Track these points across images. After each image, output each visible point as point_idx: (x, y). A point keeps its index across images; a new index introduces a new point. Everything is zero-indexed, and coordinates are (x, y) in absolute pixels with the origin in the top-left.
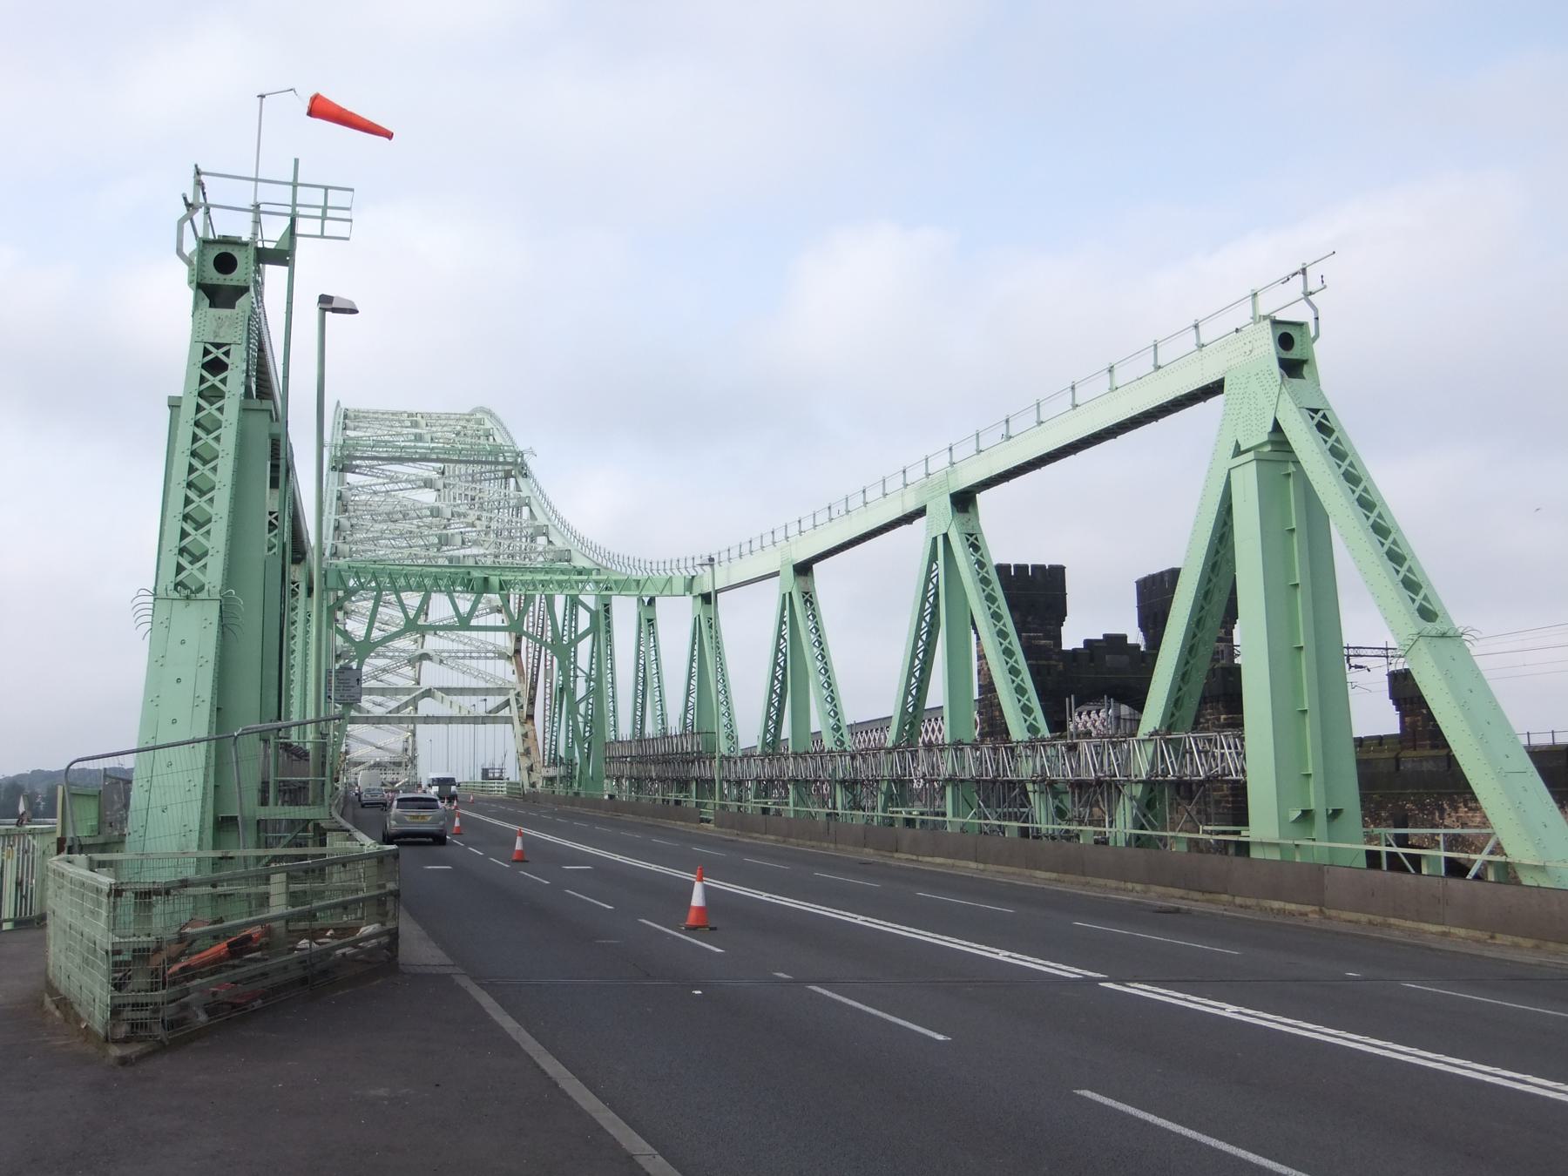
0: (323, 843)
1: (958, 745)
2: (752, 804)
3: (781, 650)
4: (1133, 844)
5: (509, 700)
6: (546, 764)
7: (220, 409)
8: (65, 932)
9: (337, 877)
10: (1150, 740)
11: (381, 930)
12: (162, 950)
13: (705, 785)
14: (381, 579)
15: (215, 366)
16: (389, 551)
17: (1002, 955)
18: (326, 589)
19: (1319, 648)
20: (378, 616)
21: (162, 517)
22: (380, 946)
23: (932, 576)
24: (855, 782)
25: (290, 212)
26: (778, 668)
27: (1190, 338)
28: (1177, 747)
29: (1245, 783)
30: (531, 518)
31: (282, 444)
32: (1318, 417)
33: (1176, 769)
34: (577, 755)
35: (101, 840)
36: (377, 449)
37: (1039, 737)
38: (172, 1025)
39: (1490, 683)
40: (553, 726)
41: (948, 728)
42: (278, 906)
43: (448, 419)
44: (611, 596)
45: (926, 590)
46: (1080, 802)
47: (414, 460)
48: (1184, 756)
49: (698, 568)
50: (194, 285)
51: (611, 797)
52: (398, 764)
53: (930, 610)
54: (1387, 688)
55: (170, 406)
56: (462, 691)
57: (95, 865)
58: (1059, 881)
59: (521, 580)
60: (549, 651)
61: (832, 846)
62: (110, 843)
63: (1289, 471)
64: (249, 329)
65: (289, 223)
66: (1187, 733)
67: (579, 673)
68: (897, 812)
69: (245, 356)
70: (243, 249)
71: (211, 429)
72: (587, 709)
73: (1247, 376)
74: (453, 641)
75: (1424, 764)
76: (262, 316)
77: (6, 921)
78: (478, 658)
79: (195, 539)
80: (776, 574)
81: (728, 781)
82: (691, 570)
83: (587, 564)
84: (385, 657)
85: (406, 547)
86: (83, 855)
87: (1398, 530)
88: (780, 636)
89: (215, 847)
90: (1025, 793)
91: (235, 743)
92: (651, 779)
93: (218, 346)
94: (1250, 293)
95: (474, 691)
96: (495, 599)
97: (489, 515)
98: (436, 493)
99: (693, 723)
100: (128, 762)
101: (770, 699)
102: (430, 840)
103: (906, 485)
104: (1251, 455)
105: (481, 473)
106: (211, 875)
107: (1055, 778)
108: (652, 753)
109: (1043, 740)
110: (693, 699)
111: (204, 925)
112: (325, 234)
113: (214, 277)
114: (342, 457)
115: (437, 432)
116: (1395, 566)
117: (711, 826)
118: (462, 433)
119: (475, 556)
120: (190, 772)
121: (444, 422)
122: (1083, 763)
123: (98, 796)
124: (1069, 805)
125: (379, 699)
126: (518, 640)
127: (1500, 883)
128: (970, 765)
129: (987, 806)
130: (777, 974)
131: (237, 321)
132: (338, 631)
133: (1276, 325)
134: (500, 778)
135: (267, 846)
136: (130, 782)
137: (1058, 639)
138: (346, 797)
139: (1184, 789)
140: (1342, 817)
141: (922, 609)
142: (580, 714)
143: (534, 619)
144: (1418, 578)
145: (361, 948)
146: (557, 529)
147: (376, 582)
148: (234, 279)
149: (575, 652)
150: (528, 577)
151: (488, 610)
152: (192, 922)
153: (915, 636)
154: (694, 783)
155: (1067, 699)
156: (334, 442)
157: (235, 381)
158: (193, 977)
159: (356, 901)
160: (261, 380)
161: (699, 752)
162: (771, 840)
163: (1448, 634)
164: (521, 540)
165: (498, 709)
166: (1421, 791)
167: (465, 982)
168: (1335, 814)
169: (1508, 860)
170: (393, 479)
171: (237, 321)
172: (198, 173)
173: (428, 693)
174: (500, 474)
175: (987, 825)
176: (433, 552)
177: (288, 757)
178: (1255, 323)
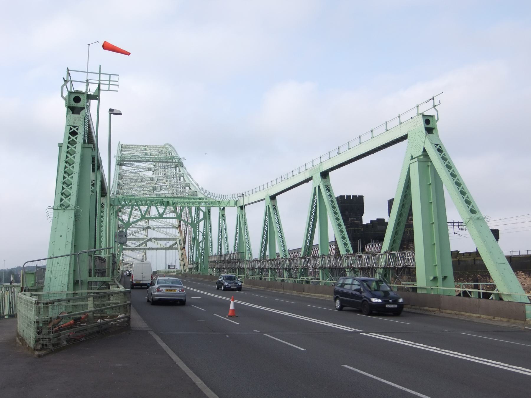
0: (109, 288)
2: (257, 277)
3: (266, 225)
5: (177, 242)
6: (189, 264)
7: (75, 147)
8: (22, 316)
13: (241, 270)
15: (74, 133)
16: (136, 192)
17: (330, 325)
23: (315, 200)
24: (290, 269)
25: (98, 83)
26: (265, 231)
29: (415, 268)
30: (184, 181)
32: (438, 147)
33: (393, 263)
34: (199, 260)
35: (35, 288)
36: (132, 158)
37: (349, 253)
38: (55, 345)
40: (191, 251)
41: (320, 252)
42: (90, 308)
43: (157, 147)
45: (313, 205)
48: (396, 259)
49: (239, 198)
50: (67, 106)
51: (211, 274)
53: (314, 211)
56: (161, 239)
59: (180, 202)
61: (282, 290)
62: (38, 289)
63: (429, 165)
65: (98, 86)
67: (200, 233)
68: (304, 279)
69: (83, 130)
70: (83, 95)
71: (72, 154)
72: (203, 245)
73: (415, 133)
74: (158, 222)
76: (90, 116)
77: (6, 315)
78: (167, 228)
79: (67, 190)
80: (264, 199)
81: (249, 269)
82: (236, 198)
83: (202, 196)
85: (142, 191)
87: (464, 184)
88: (265, 220)
89: (74, 289)
90: (345, 271)
91: (78, 256)
92: (224, 269)
93: (74, 127)
94: (416, 106)
95: (165, 239)
101: (262, 241)
103: (306, 170)
104: (416, 159)
107: (355, 267)
108: (224, 259)
109: (351, 254)
110: (237, 241)
112: (110, 90)
113: (73, 104)
114: (121, 160)
115: (152, 152)
116: (463, 196)
119: (165, 194)
121: (155, 149)
122: (363, 262)
125: (134, 242)
126: (180, 222)
127: (496, 300)
128: (327, 263)
129: (333, 276)
130: (255, 331)
131: (81, 118)
134: (174, 268)
137: (361, 220)
141: (311, 211)
142: (200, 247)
143: (185, 215)
144: (470, 200)
145: (117, 322)
146: (192, 184)
149: (199, 226)
150: (182, 201)
151: (170, 212)
153: (309, 220)
154: (238, 270)
155: (358, 241)
156: (118, 156)
157: (80, 138)
161: (239, 259)
165: (173, 245)
166: (483, 271)
168: (445, 278)
169: (499, 292)
170: (138, 168)
171: (81, 118)
172: (68, 70)
173: (150, 240)
177: (100, 261)
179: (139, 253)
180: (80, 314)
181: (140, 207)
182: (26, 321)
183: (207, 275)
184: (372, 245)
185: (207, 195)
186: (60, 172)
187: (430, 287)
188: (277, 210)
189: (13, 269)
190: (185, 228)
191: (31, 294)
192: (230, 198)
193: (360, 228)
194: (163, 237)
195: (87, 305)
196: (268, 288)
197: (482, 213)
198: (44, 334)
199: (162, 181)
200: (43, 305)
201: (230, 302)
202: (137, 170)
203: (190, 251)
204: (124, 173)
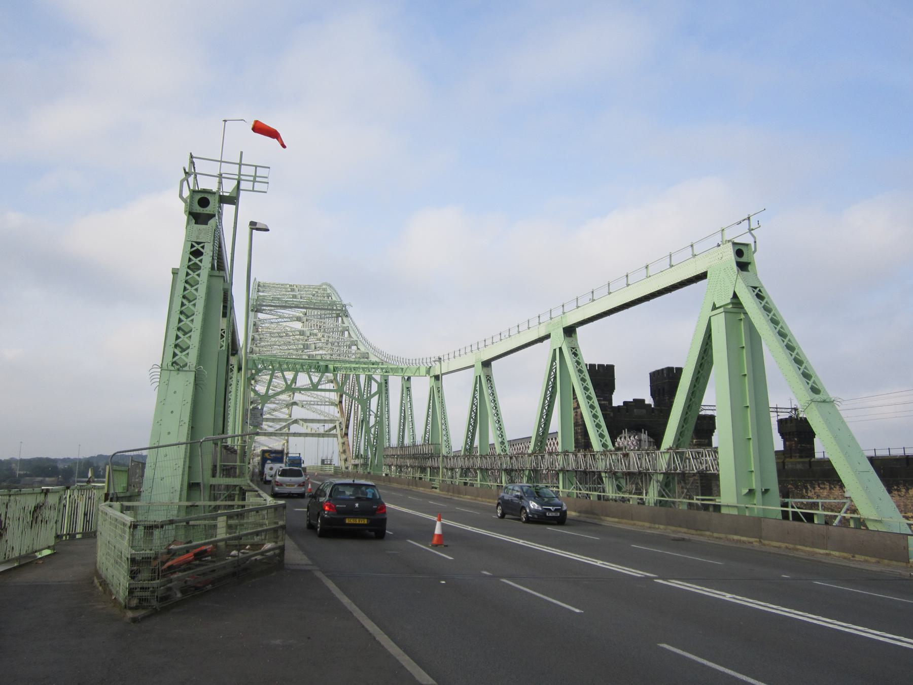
0: (244, 499)
1: (565, 453)
7: (199, 275)
9: (252, 518)
10: (667, 452)
11: (275, 547)
12: (158, 558)
13: (435, 470)
15: (197, 253)
16: (279, 351)
18: (247, 369)
22: (275, 555)
24: (512, 470)
28: (681, 456)
29: (719, 475)
32: (757, 291)
33: (681, 467)
34: (369, 453)
35: (128, 494)
38: (163, 599)
39: (849, 425)
40: (358, 439)
42: (222, 533)
44: (388, 376)
45: (550, 375)
46: (630, 481)
47: (291, 307)
48: (685, 462)
49: (433, 363)
51: (387, 475)
55: (173, 273)
56: (312, 421)
57: (125, 508)
60: (356, 402)
64: (214, 235)
67: (371, 413)
70: (213, 195)
72: (375, 431)
76: (221, 230)
77: (78, 533)
78: (321, 405)
80: (473, 366)
81: (447, 468)
83: (378, 360)
84: (274, 403)
88: (474, 397)
89: (188, 500)
92: (407, 466)
93: (198, 243)
95: (318, 421)
96: (330, 376)
97: (328, 335)
99: (429, 439)
100: (145, 453)
103: (540, 323)
104: (722, 310)
105: (325, 314)
107: (617, 470)
108: (408, 453)
110: (429, 427)
111: (181, 544)
113: (198, 209)
114: (256, 305)
117: (437, 491)
118: (316, 295)
119: (321, 355)
120: (176, 460)
121: (307, 289)
124: (624, 484)
125: (271, 424)
126: (341, 396)
127: (857, 528)
129: (581, 484)
135: (215, 499)
139: (683, 476)
141: (548, 385)
143: (349, 387)
147: (272, 366)
148: (208, 210)
150: (348, 365)
152: (175, 542)
157: (206, 261)
160: (220, 266)
161: (432, 454)
162: (468, 499)
163: (827, 401)
164: (344, 347)
165: (331, 430)
166: (797, 479)
167: (319, 574)
168: (766, 491)
173: (296, 421)
174: (334, 315)
175: (580, 493)
177: (226, 452)
179: (277, 440)
181: (285, 373)
182: (112, 554)
184: (625, 438)
186: (173, 312)
188: (492, 382)
190: (349, 405)
191: (122, 505)
193: (609, 413)
194: (315, 418)
196: (477, 498)
199: (315, 337)
201: (435, 523)
203: (357, 441)
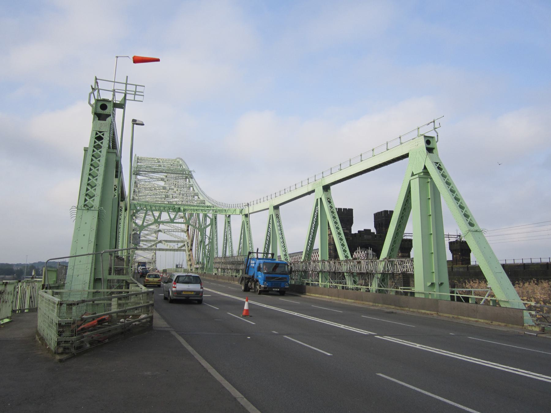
0: (128, 288)
4: (378, 292)
7: (100, 152)
8: (43, 315)
9: (133, 299)
10: (383, 261)
11: (147, 316)
14: (148, 207)
15: (99, 138)
18: (130, 209)
19: (437, 234)
20: (146, 218)
21: (82, 171)
22: (147, 322)
27: (416, 132)
29: (414, 274)
31: (119, 163)
32: (438, 165)
34: (205, 261)
35: (57, 285)
38: (78, 348)
42: (114, 308)
45: (314, 214)
49: (244, 207)
50: (94, 113)
52: (150, 263)
54: (449, 247)
58: (355, 303)
60: (197, 230)
63: (429, 181)
64: (110, 127)
66: (395, 259)
67: (206, 237)
69: (109, 135)
72: (209, 248)
73: (416, 152)
75: (460, 269)
76: (114, 124)
77: (26, 309)
78: (176, 232)
79: (89, 202)
80: (268, 209)
84: (147, 231)
86: (51, 290)
89: (94, 288)
91: (102, 256)
92: (228, 269)
93: (100, 132)
95: (174, 242)
96: (181, 214)
98: (164, 183)
100: (67, 260)
102: (157, 286)
104: (417, 176)
105: (178, 177)
106: (93, 299)
108: (228, 261)
109: (350, 260)
110: (242, 245)
112: (135, 100)
113: (100, 111)
119: (176, 201)
121: (167, 161)
122: (362, 267)
123: (56, 271)
124: (358, 279)
125: (145, 243)
127: (494, 306)
129: (332, 280)
132: (134, 222)
133: (426, 137)
134: (181, 268)
135: (111, 288)
136: (67, 267)
138: (134, 272)
140: (443, 285)
141: (313, 220)
143: (193, 221)
144: (469, 214)
146: (201, 194)
150: (192, 208)
157: (105, 143)
158: (85, 332)
159: (140, 307)
161: (243, 261)
165: (182, 247)
166: (459, 277)
167: (174, 333)
168: (441, 284)
173: (160, 242)
174: (184, 177)
175: (332, 285)
176: (163, 200)
177: (118, 260)
178: (419, 137)
179: (149, 253)
180: (104, 315)
183: (212, 274)
184: (359, 252)
185: (215, 205)
187: (428, 292)
189: (35, 263)
190: (193, 232)
191: (53, 291)
192: (240, 206)
193: (349, 237)
195: (110, 305)
197: (479, 226)
198: (67, 337)
200: (67, 306)
201: (244, 302)
202: (151, 180)
203: (198, 254)
204: (139, 182)
